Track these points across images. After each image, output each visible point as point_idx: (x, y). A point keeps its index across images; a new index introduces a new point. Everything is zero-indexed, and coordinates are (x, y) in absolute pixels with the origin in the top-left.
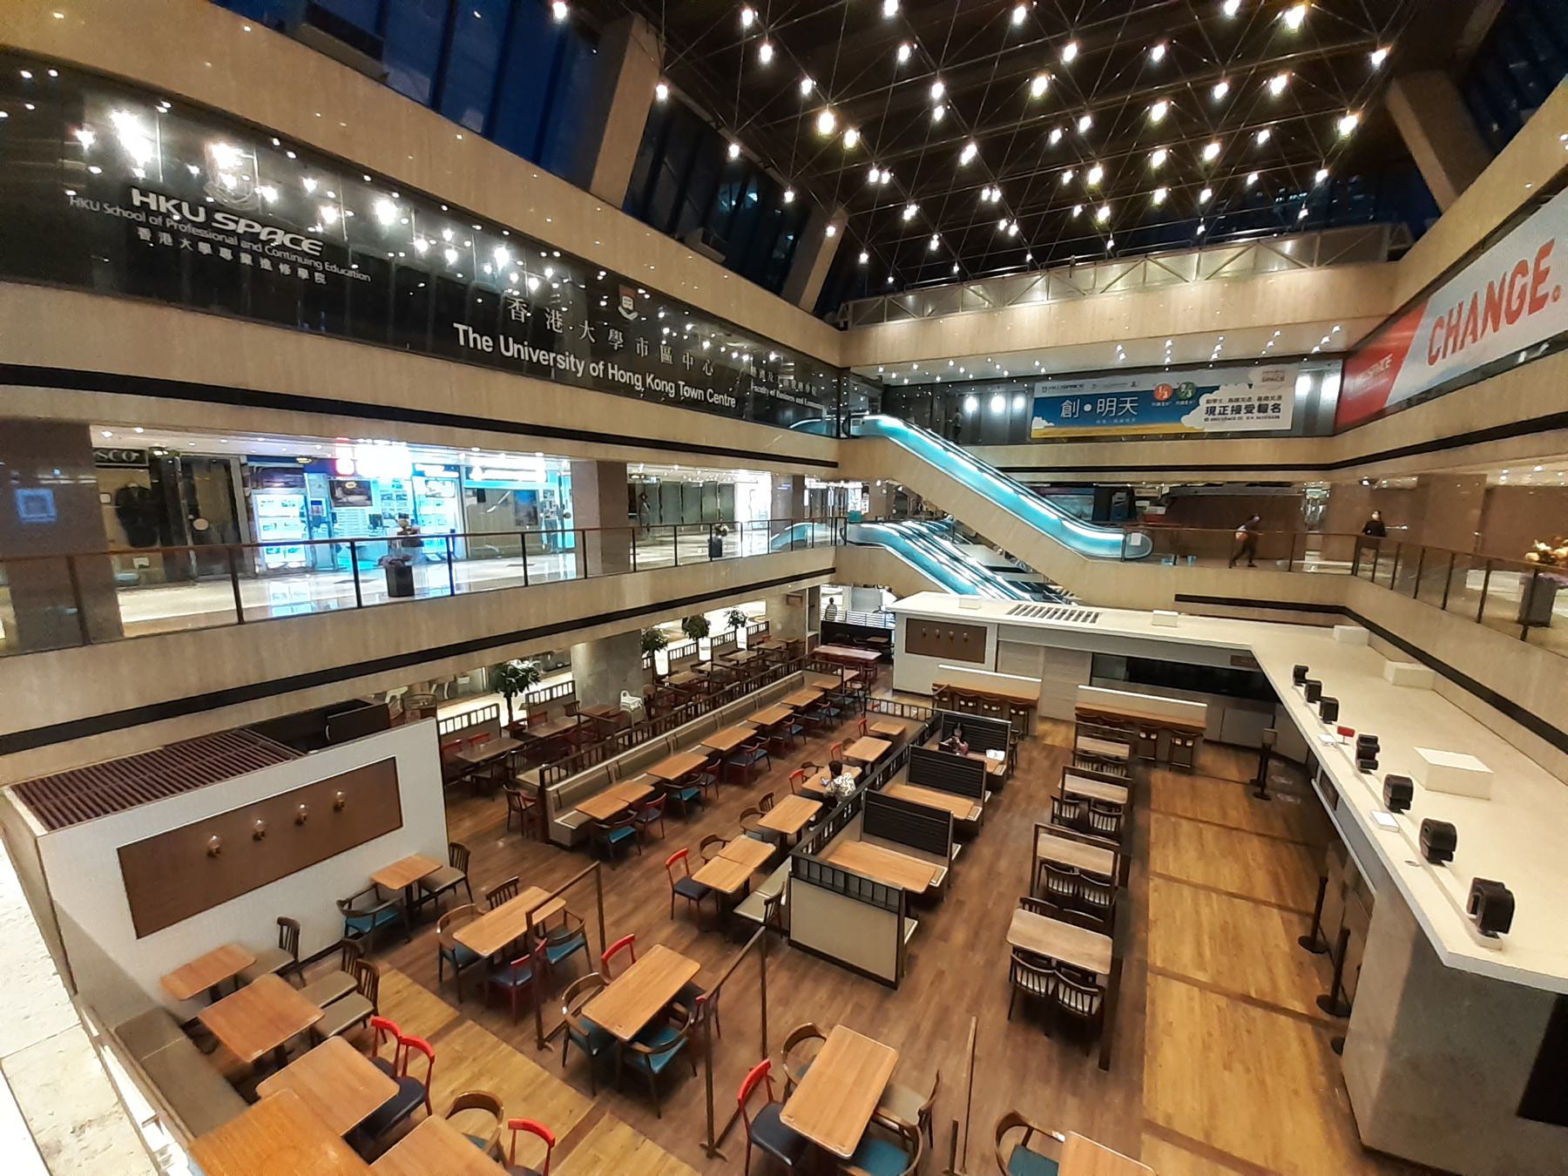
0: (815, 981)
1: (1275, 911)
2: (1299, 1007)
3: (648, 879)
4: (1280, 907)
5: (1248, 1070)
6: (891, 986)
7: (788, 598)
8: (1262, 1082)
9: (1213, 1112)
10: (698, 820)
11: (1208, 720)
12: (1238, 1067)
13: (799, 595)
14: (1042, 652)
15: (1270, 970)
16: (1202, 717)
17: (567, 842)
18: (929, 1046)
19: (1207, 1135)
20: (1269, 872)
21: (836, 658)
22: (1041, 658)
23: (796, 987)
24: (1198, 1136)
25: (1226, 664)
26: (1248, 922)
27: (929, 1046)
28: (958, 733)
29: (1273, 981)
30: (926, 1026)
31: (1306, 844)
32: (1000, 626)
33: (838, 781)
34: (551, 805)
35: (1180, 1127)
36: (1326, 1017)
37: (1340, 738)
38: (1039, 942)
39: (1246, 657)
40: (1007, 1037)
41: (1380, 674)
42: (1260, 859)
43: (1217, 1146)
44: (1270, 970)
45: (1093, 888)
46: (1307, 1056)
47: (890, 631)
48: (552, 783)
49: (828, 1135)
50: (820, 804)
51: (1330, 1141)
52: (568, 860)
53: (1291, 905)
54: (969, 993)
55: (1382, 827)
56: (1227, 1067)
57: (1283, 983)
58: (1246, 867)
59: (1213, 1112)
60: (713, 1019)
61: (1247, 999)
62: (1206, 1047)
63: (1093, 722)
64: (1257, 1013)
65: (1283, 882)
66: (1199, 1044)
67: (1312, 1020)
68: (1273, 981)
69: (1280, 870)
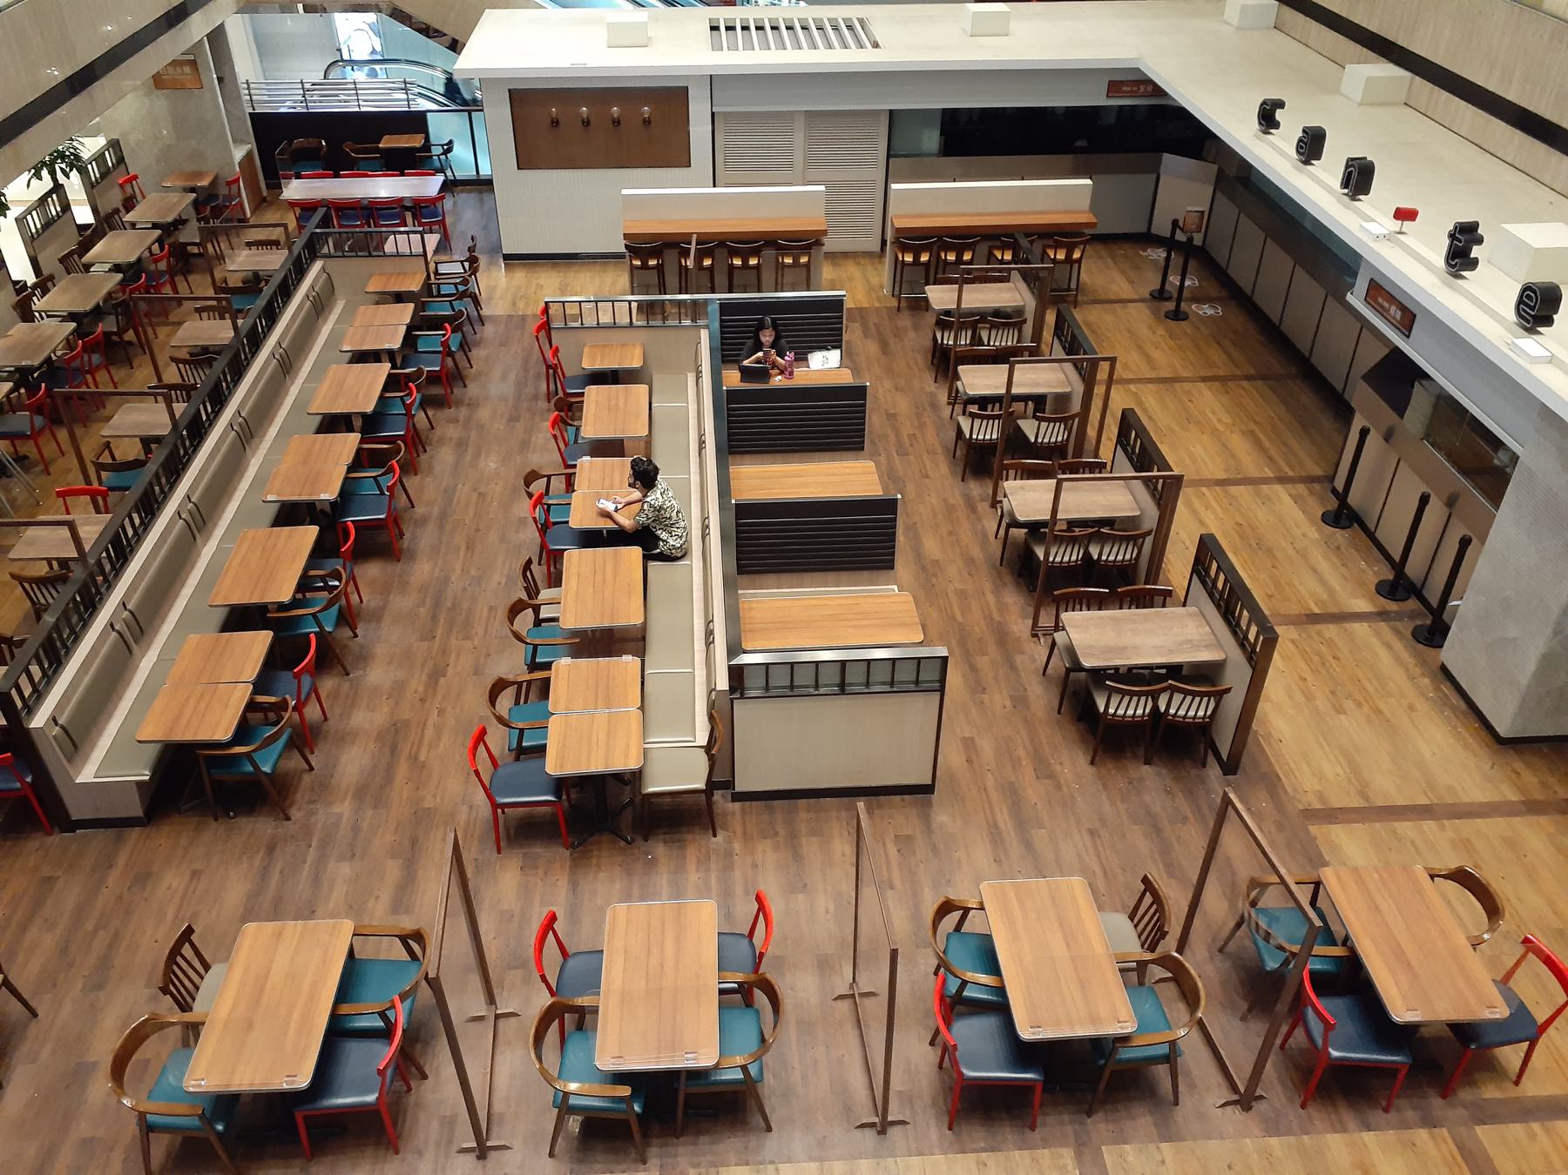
0: (814, 833)
1: (1278, 488)
2: (1362, 605)
3: (380, 802)
4: (1282, 480)
5: (1359, 705)
6: (928, 789)
7: (158, 81)
8: (1379, 712)
9: (1355, 769)
10: (364, 658)
11: (1093, 208)
12: (1349, 705)
13: (191, 62)
14: (800, 124)
15: (1314, 570)
16: (1085, 203)
17: (137, 811)
18: (1028, 845)
19: (1363, 794)
20: (1243, 433)
21: (373, 210)
22: (799, 138)
23: (797, 857)
24: (1357, 802)
25: (1096, 97)
26: (1260, 516)
27: (1028, 845)
28: (767, 337)
29: (1323, 582)
30: (1004, 820)
31: (1263, 378)
32: (713, 81)
33: (655, 497)
34: (52, 755)
35: (1337, 802)
36: (1393, 606)
37: (1396, 225)
38: (1122, 650)
39: (1135, 82)
40: (1105, 788)
41: (1335, 89)
42: (1227, 419)
43: (1379, 804)
44: (1314, 570)
45: (1102, 539)
46: (1398, 659)
47: (422, 116)
48: (31, 710)
49: (1094, 1020)
51: (1466, 747)
52: (163, 840)
53: (1290, 473)
54: (1021, 752)
55: (1534, 360)
56: (1340, 710)
57: (1335, 582)
58: (1215, 433)
59: (1355, 769)
60: (102, 939)
61: (1313, 619)
62: (1309, 697)
63: (930, 252)
64: (1330, 630)
65: (1267, 444)
66: (1299, 697)
67: (1383, 615)
68: (1323, 582)
69: (1254, 427)
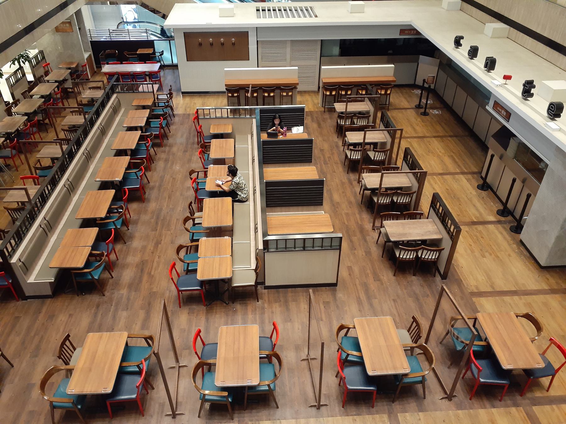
0: (294, 300)
1: (461, 176)
2: (492, 218)
3: (137, 289)
4: (463, 173)
5: (491, 254)
6: (335, 285)
7: (57, 29)
8: (498, 257)
9: (489, 278)
10: (131, 237)
11: (395, 75)
12: (487, 254)
13: (69, 22)
14: (289, 45)
15: (474, 206)
16: (392, 73)
17: (49, 293)
18: (371, 305)
19: (492, 287)
20: (449, 156)
21: (135, 76)
22: (288, 50)
23: (288, 309)
24: (490, 290)
25: (396, 35)
26: (455, 186)
27: (371, 305)
28: (277, 122)
29: (477, 210)
30: (363, 296)
31: (456, 136)
32: (257, 29)
33: (236, 179)
34: (19, 273)
35: (483, 289)
36: (503, 219)
37: (504, 81)
38: (405, 235)
39: (410, 30)
40: (399, 284)
41: (482, 32)
42: (443, 151)
43: (498, 290)
44: (474, 206)
45: (398, 194)
46: (505, 238)
47: (152, 42)
48: (11, 256)
49: (395, 368)
50: (113, 191)
51: (529, 270)
52: (59, 303)
53: (466, 171)
54: (369, 271)
55: (554, 130)
56: (484, 256)
57: (482, 210)
58: (439, 156)
59: (489, 278)
60: (37, 339)
61: (474, 223)
62: (472, 251)
63: (336, 91)
64: (480, 227)
65: (457, 160)
66: (469, 251)
67: (499, 222)
68: (477, 210)
69: (453, 154)
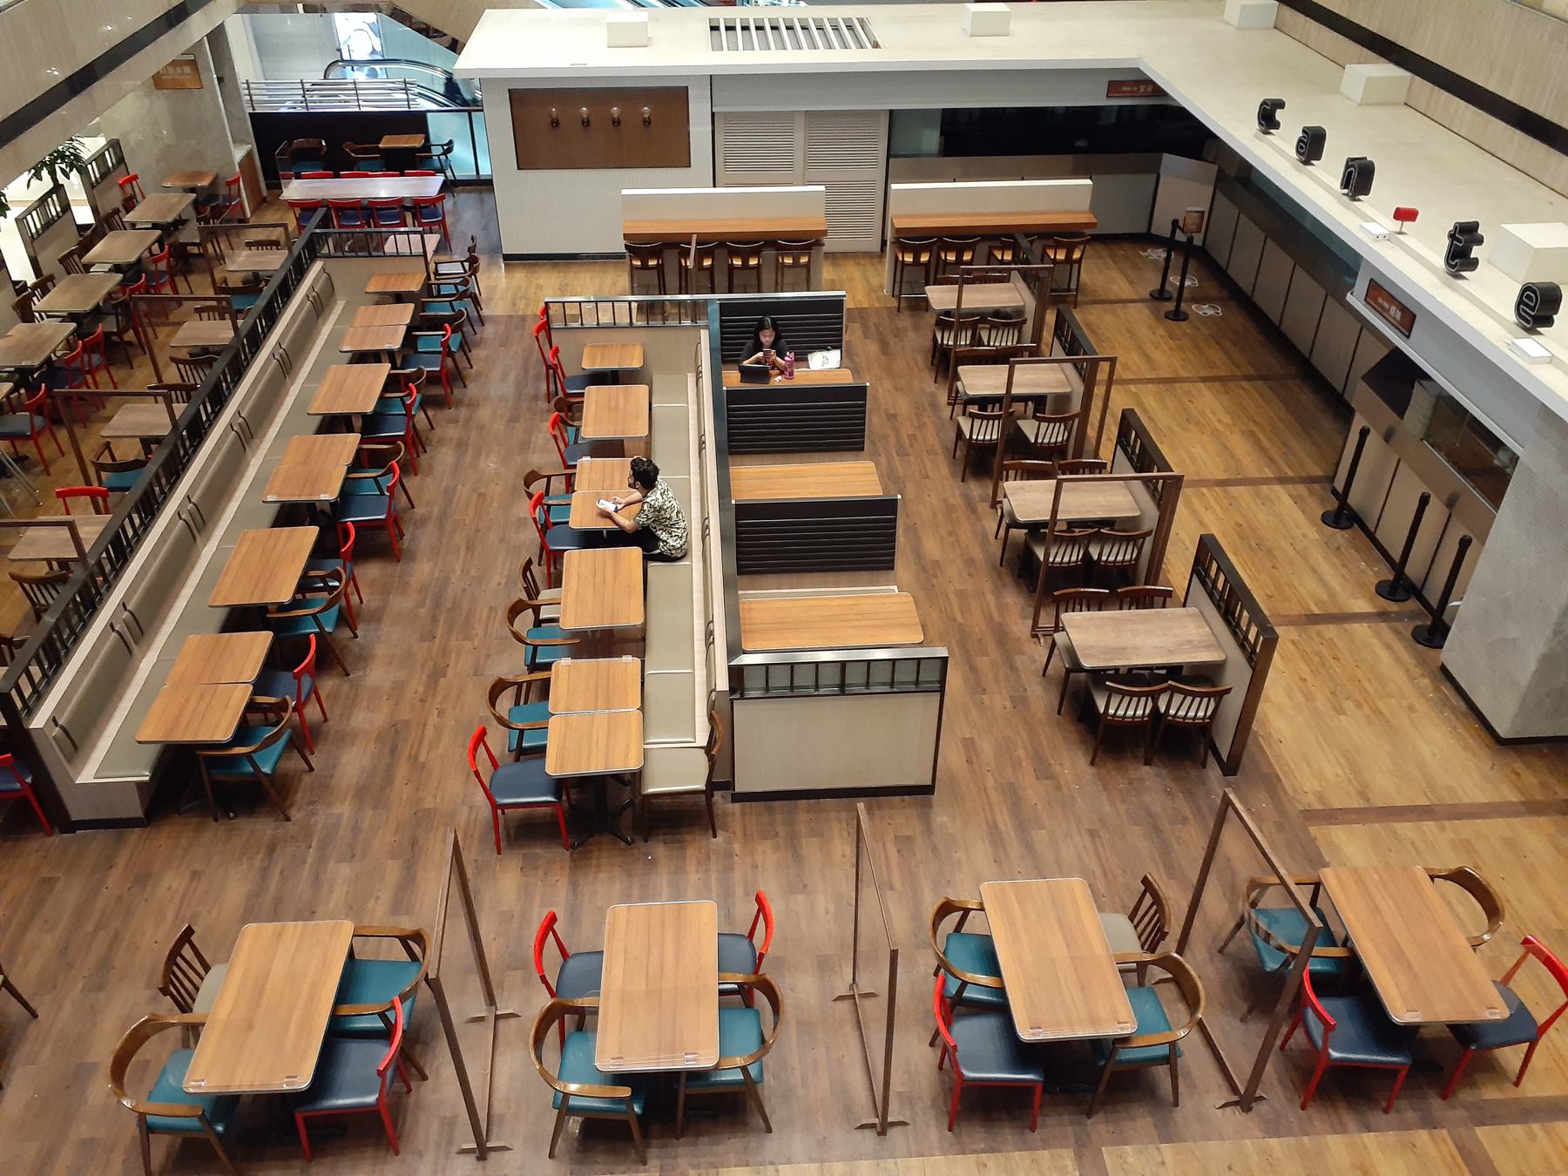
0: (814, 833)
1: (1278, 488)
2: (1362, 605)
3: (380, 803)
4: (1282, 480)
5: (1359, 706)
6: (928, 790)
7: (158, 81)
8: (1379, 713)
9: (1355, 770)
10: (364, 658)
11: (1093, 208)
12: (1349, 705)
13: (191, 62)
14: (800, 124)
15: (1314, 571)
16: (1085, 204)
17: (137, 811)
18: (1028, 846)
19: (1363, 795)
20: (1243, 433)
21: (373, 211)
22: (799, 138)
23: (797, 857)
24: (1357, 803)
25: (1096, 98)
26: (1260, 516)
27: (1028, 846)
28: (767, 337)
29: (1323, 582)
30: (1004, 821)
31: (1263, 378)
32: (713, 81)
33: (655, 498)
34: (52, 756)
35: (1337, 803)
36: (1393, 607)
37: (1396, 225)
38: (1122, 651)
39: (1135, 82)
40: (1105, 788)
41: (1335, 89)
42: (1227, 419)
43: (1379, 804)
44: (1314, 571)
45: (1102, 539)
46: (1398, 659)
47: (422, 116)
48: (31, 711)
49: (1094, 1021)
51: (1466, 747)
52: (163, 840)
53: (1290, 474)
54: (1021, 753)
55: (1534, 360)
56: (1340, 711)
57: (1335, 583)
58: (1215, 434)
59: (1355, 770)
60: (102, 940)
61: (1313, 619)
62: (1309, 697)
63: (930, 253)
64: (1330, 631)
65: (1267, 444)
66: (1299, 697)
67: (1383, 616)
68: (1323, 582)
69: (1254, 427)
